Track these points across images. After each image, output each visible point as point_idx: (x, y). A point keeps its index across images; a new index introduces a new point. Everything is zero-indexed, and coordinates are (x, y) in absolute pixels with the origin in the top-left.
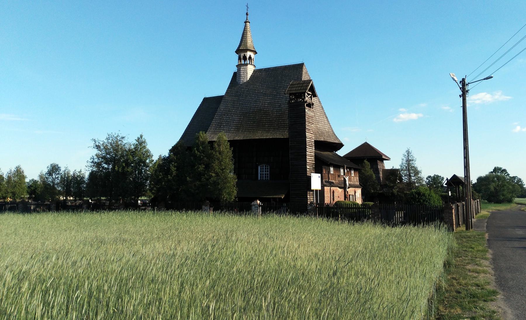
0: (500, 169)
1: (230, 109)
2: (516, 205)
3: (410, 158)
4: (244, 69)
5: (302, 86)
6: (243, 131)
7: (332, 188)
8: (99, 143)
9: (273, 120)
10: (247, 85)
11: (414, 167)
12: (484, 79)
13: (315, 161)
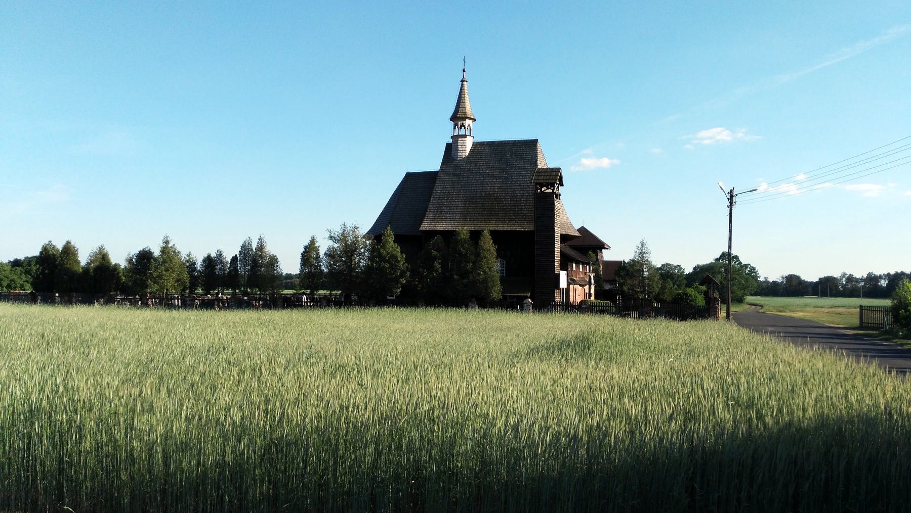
1: (450, 191)
2: (749, 306)
3: (644, 251)
4: (462, 142)
5: (551, 175)
6: (472, 220)
7: (575, 286)
8: (335, 234)
9: (507, 209)
10: (467, 162)
11: (647, 261)
12: (750, 191)
13: (560, 257)
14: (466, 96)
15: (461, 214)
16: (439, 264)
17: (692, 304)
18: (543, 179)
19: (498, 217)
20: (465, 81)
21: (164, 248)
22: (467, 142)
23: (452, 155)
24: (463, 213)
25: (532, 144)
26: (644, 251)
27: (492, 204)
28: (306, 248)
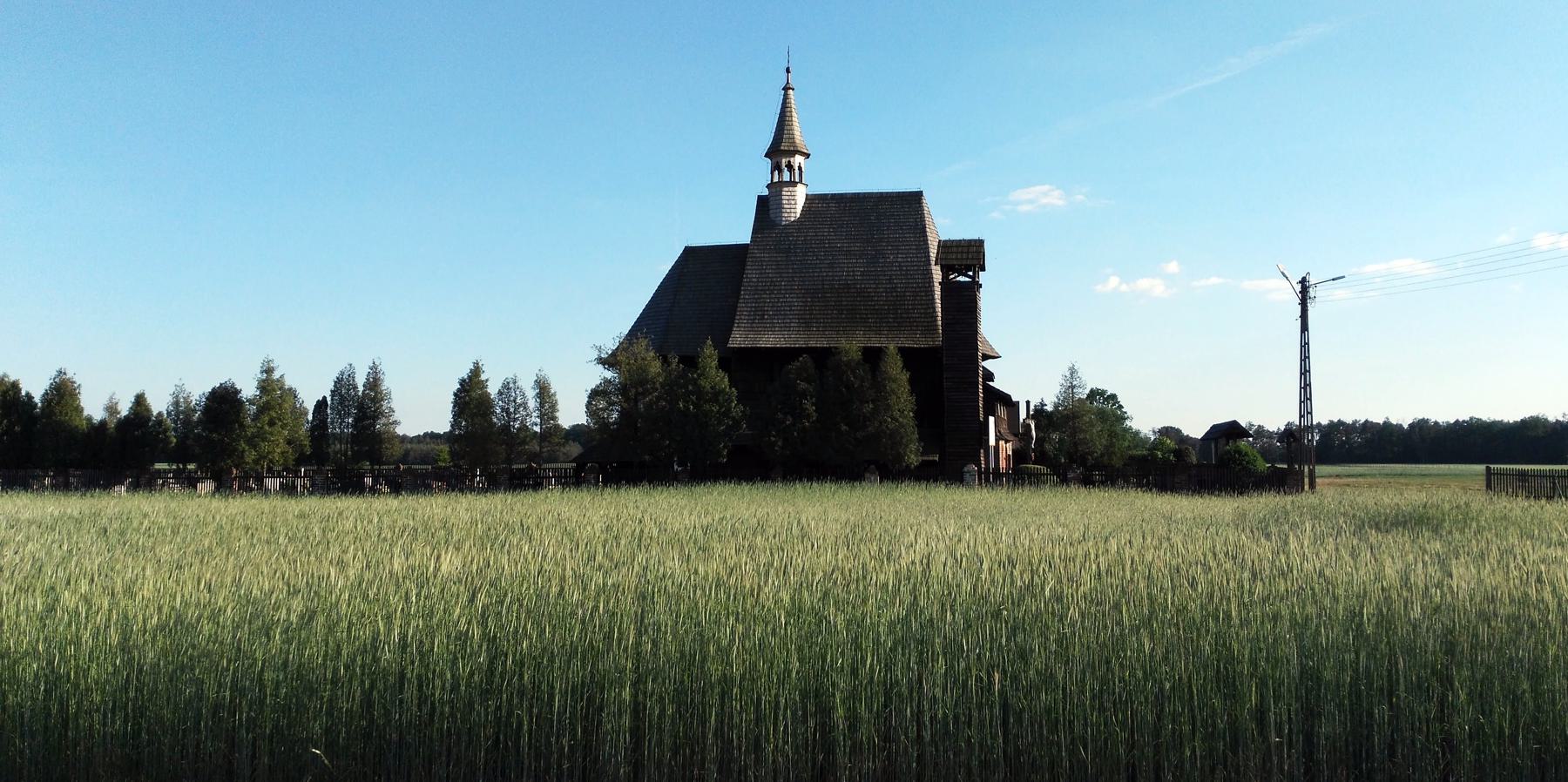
0: (1102, 393)
4: (789, 193)
12: (1333, 280)
14: (794, 114)
15: (798, 319)
16: (813, 404)
17: (1250, 469)
18: (957, 259)
19: (868, 324)
20: (790, 88)
21: (264, 381)
22: (797, 193)
23: (772, 216)
24: (803, 317)
25: (913, 200)
26: (1075, 383)
27: (854, 301)
28: (462, 382)
